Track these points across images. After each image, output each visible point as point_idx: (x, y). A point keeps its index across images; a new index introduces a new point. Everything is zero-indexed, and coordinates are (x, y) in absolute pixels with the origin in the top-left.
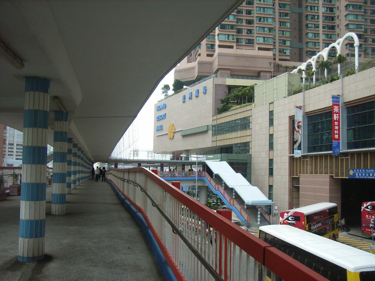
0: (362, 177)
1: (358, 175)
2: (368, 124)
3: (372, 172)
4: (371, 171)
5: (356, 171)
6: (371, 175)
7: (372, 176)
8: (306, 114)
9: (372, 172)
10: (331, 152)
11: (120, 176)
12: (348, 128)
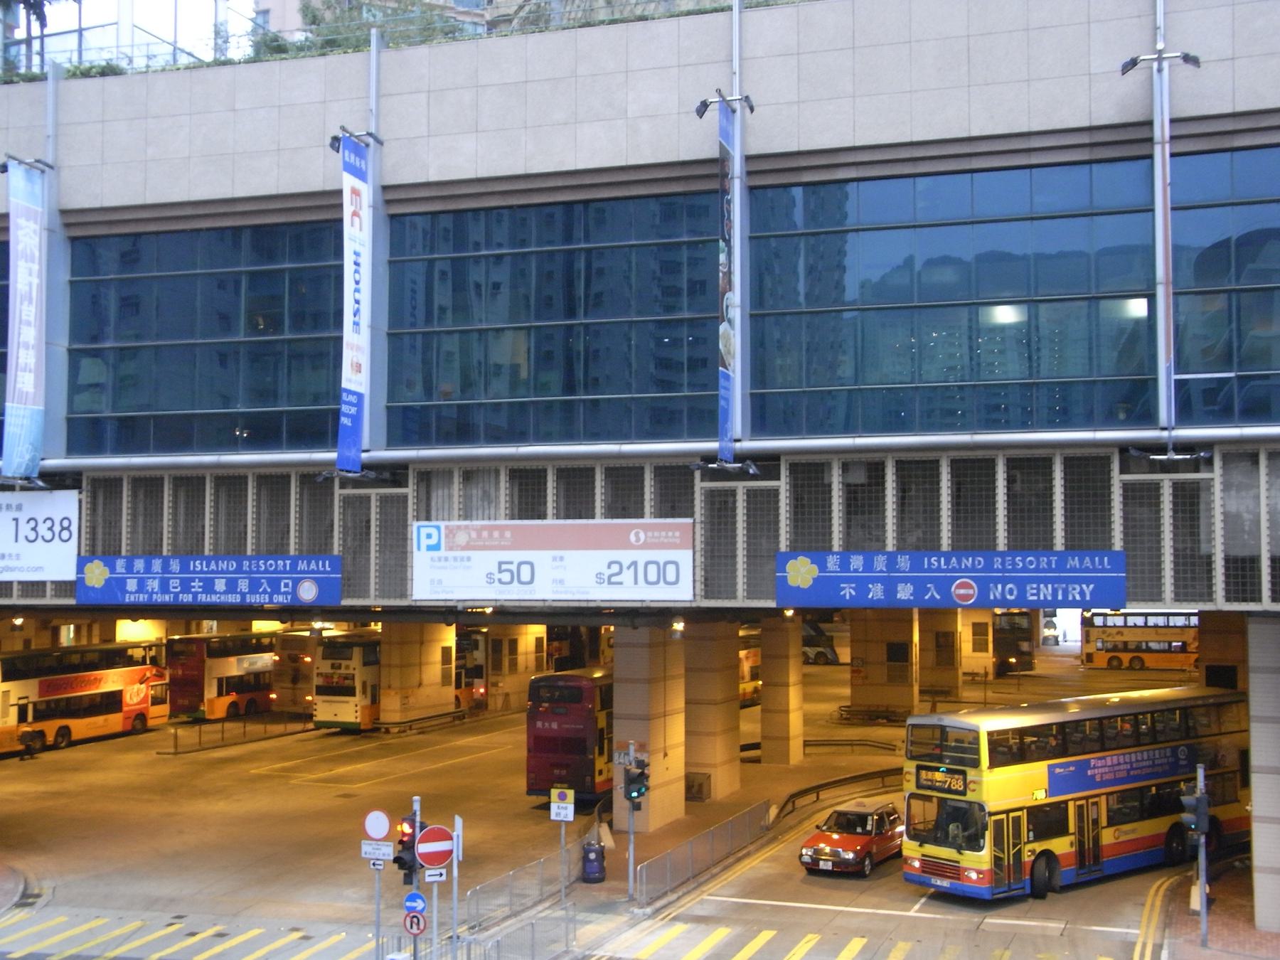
0: (167, 598)
1: (141, 587)
2: (204, 337)
3: (228, 572)
4: (223, 565)
5: (129, 568)
6: (220, 585)
7: (225, 593)
8: (391, 196)
9: (228, 572)
10: (332, 456)
11: (677, 780)
12: (75, 346)
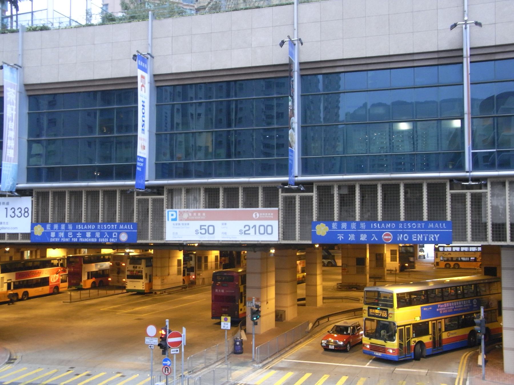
0: (67, 240)
1: (57, 235)
2: (82, 135)
3: (91, 229)
4: (90, 227)
5: (52, 228)
6: (88, 235)
7: (90, 238)
8: (157, 79)
9: (91, 229)
10: (133, 183)
11: (272, 313)
12: (30, 139)
